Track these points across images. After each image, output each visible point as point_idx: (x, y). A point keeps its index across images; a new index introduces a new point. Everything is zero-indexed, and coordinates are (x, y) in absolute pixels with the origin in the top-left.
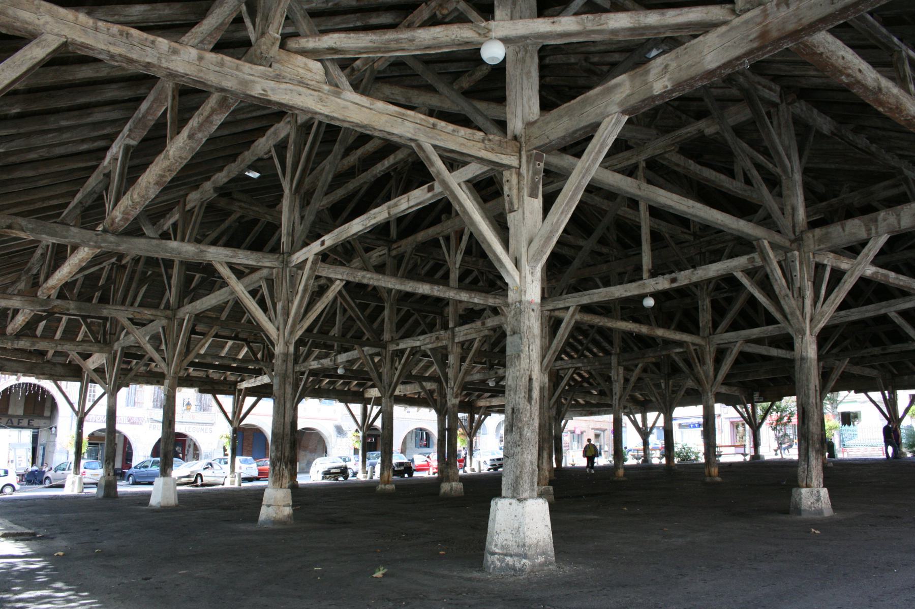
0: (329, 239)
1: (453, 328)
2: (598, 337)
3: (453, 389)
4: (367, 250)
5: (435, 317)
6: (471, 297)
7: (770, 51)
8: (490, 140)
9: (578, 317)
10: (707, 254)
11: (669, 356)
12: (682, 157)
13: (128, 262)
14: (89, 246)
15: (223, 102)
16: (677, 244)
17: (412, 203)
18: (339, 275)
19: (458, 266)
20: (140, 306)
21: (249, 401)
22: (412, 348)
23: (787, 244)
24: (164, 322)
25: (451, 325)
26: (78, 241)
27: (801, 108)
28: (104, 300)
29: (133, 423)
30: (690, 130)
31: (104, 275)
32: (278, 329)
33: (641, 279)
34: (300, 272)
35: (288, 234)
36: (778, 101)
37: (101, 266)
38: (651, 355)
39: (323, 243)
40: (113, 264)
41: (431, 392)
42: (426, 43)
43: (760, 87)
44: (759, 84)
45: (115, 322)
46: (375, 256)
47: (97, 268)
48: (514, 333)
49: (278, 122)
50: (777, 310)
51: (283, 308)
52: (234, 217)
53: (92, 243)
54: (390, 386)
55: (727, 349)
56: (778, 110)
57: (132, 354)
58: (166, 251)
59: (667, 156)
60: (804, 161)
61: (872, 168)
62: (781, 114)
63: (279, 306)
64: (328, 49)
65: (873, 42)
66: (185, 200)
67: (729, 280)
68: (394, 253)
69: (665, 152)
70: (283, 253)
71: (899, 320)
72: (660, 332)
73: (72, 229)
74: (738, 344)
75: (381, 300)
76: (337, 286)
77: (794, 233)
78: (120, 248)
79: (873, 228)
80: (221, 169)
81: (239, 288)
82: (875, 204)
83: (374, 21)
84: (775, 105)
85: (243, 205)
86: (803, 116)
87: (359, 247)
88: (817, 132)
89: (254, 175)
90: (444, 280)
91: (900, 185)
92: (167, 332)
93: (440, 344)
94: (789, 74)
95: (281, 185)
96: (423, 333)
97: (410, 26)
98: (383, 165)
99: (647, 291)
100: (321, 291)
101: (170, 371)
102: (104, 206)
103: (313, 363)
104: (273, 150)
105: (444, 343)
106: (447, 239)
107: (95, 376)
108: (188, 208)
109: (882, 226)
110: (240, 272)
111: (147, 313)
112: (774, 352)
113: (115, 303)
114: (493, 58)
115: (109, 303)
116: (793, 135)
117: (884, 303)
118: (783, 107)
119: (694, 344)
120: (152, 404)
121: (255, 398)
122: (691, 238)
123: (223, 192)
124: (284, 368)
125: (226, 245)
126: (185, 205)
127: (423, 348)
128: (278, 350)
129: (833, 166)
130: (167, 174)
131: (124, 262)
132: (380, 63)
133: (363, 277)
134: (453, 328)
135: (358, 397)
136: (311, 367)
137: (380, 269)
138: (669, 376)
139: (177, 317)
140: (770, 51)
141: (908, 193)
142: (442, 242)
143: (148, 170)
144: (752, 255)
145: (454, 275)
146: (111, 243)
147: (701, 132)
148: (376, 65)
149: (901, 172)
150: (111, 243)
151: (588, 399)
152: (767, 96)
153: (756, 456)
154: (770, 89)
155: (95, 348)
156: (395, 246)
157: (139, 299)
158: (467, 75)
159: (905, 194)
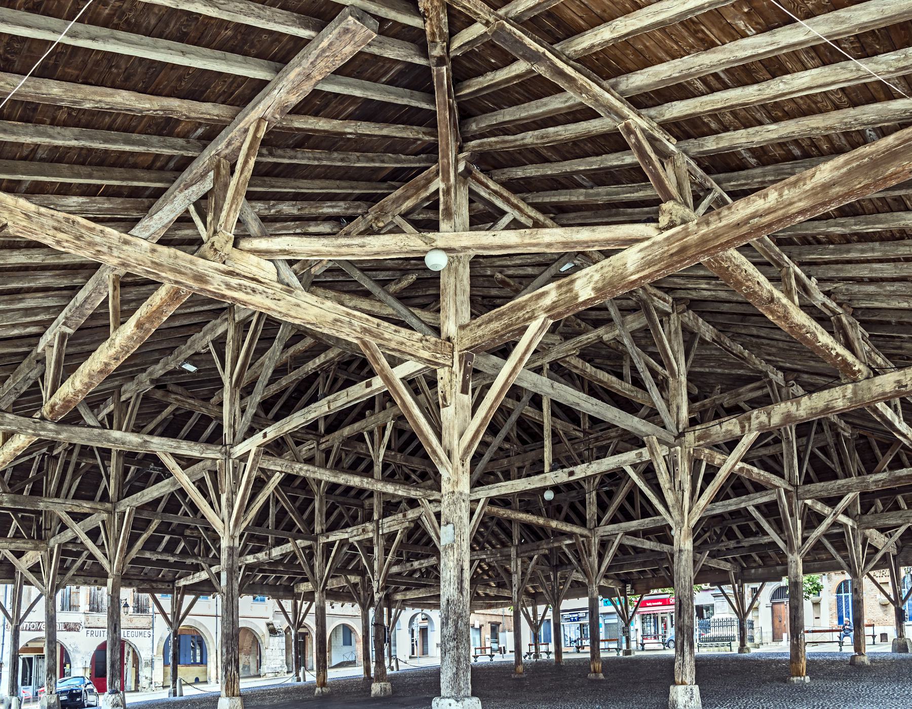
0: (272, 432)
1: (378, 521)
2: (496, 529)
3: (378, 581)
4: (298, 444)
5: (357, 510)
6: (395, 490)
7: (687, 264)
8: (427, 340)
9: (486, 509)
10: (595, 450)
11: (560, 548)
12: (581, 361)
13: (60, 453)
14: (27, 434)
15: (175, 295)
16: (569, 440)
17: (350, 399)
18: (279, 467)
19: (381, 459)
20: (74, 498)
21: (188, 599)
22: (341, 540)
23: (672, 440)
24: (105, 516)
25: (376, 517)
26: (14, 428)
27: (690, 317)
28: (37, 491)
29: (70, 630)
30: (591, 336)
31: (35, 466)
32: (223, 521)
33: (543, 472)
34: (243, 464)
35: (230, 426)
36: (670, 310)
37: (32, 456)
38: (545, 546)
39: (265, 435)
40: (44, 454)
41: (355, 585)
42: (375, 249)
43: (655, 298)
44: (655, 295)
45: (50, 515)
46: (304, 449)
47: (27, 458)
48: (448, 523)
49: (216, 319)
50: (660, 502)
51: (228, 499)
52: (170, 409)
53: (30, 431)
54: (321, 580)
55: (609, 541)
56: (669, 319)
57: (71, 551)
58: (109, 441)
59: (567, 359)
60: (689, 364)
61: (741, 372)
62: (672, 322)
63: (224, 498)
64: (281, 251)
65: (767, 259)
66: (120, 391)
67: (616, 476)
68: (323, 446)
69: (567, 356)
70: (225, 445)
71: (756, 514)
72: (554, 524)
73: (7, 415)
74: (619, 537)
75: (310, 492)
76: (276, 479)
77: (678, 428)
78: (60, 437)
79: (747, 425)
80: (157, 362)
81: (184, 479)
82: (742, 404)
83: (312, 229)
84: (668, 314)
85: (179, 397)
86: (690, 324)
87: (290, 441)
88: (701, 338)
89: (190, 368)
90: (368, 472)
91: (766, 387)
92: (108, 526)
93: (366, 537)
94: (682, 287)
95: (220, 379)
96: (347, 526)
97: (348, 234)
98: (315, 363)
99: (548, 483)
100: (259, 484)
101: (112, 568)
102: (41, 393)
103: (248, 557)
104: (211, 345)
105: (371, 535)
106: (371, 433)
107: (31, 577)
108: (123, 398)
109: (755, 423)
110: (186, 462)
111: (85, 507)
112: (648, 545)
113: (49, 496)
114: (436, 265)
115: (42, 495)
116: (682, 342)
117: (744, 497)
118: (674, 316)
119: (582, 536)
120: (88, 607)
121: (193, 597)
122: (581, 435)
123: (159, 384)
124: (230, 562)
125: (162, 435)
126: (120, 396)
127: (351, 540)
128: (224, 543)
129: (707, 370)
130: (113, 362)
131: (55, 453)
132: (317, 268)
133: (301, 469)
134: (378, 521)
135: (288, 591)
136: (247, 562)
137: (310, 461)
138: (555, 568)
139: (117, 510)
140: (687, 264)
141: (771, 395)
142: (366, 436)
143: (91, 357)
144: (640, 450)
145: (378, 469)
146: (49, 431)
147: (600, 338)
148: (313, 270)
149: (767, 376)
150: (51, 430)
151: (488, 591)
152: (661, 306)
153: (806, 644)
154: (664, 300)
155: (29, 546)
156: (323, 440)
157: (73, 491)
158: (393, 283)
159: (768, 395)
